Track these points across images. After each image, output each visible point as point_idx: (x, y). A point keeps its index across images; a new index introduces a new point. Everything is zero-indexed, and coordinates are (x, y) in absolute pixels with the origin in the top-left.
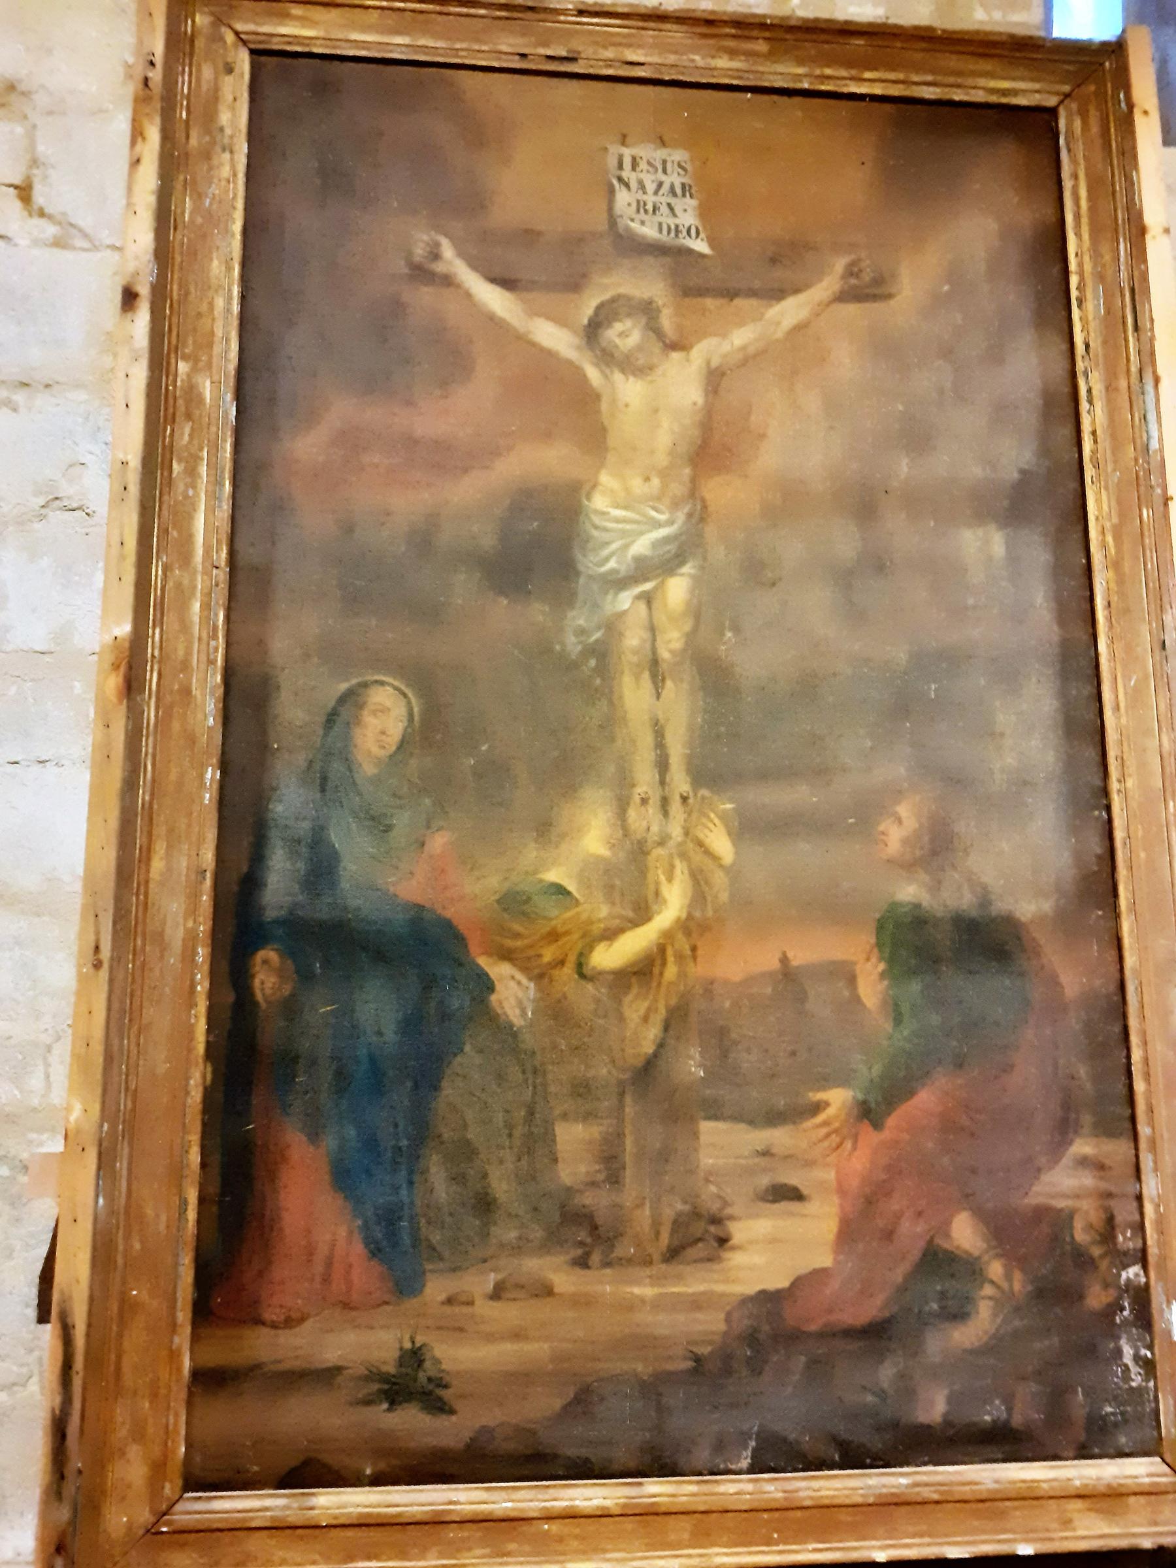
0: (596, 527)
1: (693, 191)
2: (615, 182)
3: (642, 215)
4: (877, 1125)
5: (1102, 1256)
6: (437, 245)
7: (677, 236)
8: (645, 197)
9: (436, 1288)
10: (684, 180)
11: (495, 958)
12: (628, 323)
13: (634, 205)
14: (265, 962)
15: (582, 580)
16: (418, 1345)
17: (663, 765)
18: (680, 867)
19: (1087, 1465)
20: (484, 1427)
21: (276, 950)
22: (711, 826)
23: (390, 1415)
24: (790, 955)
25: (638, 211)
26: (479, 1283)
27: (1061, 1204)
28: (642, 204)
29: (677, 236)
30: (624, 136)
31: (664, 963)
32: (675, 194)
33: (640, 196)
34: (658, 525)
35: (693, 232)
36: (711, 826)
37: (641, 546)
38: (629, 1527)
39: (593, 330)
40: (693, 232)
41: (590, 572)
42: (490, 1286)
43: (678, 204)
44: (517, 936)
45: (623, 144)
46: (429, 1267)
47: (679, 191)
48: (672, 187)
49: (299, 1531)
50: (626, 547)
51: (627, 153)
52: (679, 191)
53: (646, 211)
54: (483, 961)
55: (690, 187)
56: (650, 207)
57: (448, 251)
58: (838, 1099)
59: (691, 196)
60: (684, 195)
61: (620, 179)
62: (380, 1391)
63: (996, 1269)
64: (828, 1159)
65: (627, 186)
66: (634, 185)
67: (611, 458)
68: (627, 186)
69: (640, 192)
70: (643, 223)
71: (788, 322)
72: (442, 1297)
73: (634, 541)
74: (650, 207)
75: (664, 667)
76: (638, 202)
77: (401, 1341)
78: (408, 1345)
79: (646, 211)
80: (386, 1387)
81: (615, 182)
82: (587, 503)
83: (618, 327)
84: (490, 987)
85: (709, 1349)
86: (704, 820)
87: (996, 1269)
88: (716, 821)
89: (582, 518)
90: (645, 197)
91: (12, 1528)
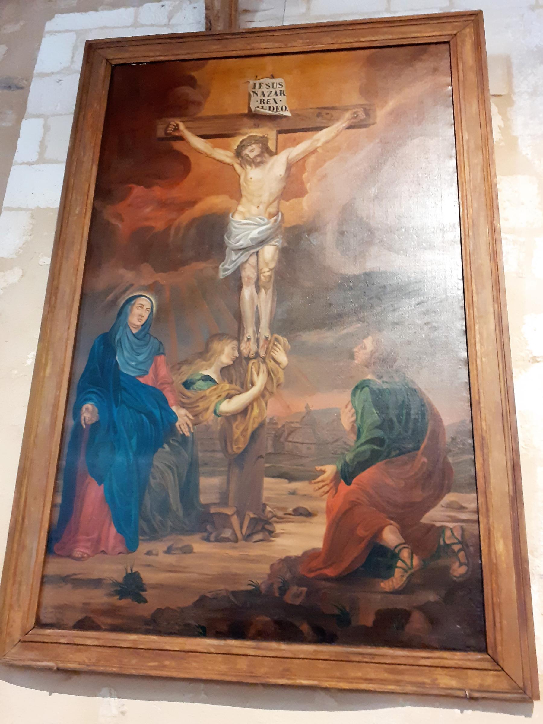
0: (235, 228)
1: (285, 93)
2: (252, 93)
3: (262, 105)
4: (348, 483)
5: (460, 550)
6: (178, 125)
7: (277, 111)
8: (264, 98)
9: (143, 547)
10: (281, 89)
11: (179, 406)
12: (254, 146)
13: (259, 101)
14: (87, 409)
15: (228, 249)
16: (133, 572)
17: (258, 323)
18: (263, 367)
19: (489, 546)
20: (158, 609)
21: (91, 404)
22: (278, 350)
23: (119, 601)
24: (310, 405)
25: (261, 103)
26: (160, 547)
27: (438, 524)
28: (262, 100)
29: (277, 111)
30: (257, 76)
31: (253, 409)
32: (277, 95)
33: (262, 98)
34: (260, 225)
35: (284, 108)
36: (278, 350)
37: (255, 233)
38: (220, 659)
39: (238, 154)
40: (284, 108)
41: (231, 246)
42: (165, 549)
43: (278, 98)
44: (189, 398)
45: (256, 79)
46: (141, 538)
47: (278, 93)
48: (276, 93)
49: (79, 647)
50: (249, 234)
51: (257, 82)
52: (278, 93)
53: (264, 103)
54: (174, 408)
55: (284, 92)
56: (265, 102)
57: (182, 127)
58: (330, 470)
59: (284, 95)
60: (281, 95)
61: (254, 92)
62: (116, 591)
63: (405, 554)
64: (324, 497)
65: (257, 94)
66: (259, 93)
67: (244, 200)
68: (257, 94)
69: (262, 96)
70: (262, 107)
71: (323, 140)
72: (145, 552)
73: (251, 232)
74: (265, 102)
75: (261, 283)
76: (261, 100)
77: (126, 570)
78: (129, 572)
79: (264, 103)
80: (119, 589)
81: (252, 93)
82: (231, 217)
83: (250, 148)
84: (176, 419)
85: (262, 581)
86: (275, 347)
87: (405, 554)
88: (280, 347)
89: (230, 224)
90: (264, 98)
91: (199, 104)
